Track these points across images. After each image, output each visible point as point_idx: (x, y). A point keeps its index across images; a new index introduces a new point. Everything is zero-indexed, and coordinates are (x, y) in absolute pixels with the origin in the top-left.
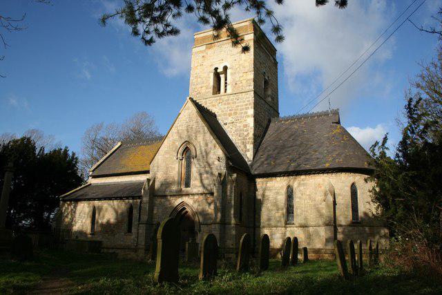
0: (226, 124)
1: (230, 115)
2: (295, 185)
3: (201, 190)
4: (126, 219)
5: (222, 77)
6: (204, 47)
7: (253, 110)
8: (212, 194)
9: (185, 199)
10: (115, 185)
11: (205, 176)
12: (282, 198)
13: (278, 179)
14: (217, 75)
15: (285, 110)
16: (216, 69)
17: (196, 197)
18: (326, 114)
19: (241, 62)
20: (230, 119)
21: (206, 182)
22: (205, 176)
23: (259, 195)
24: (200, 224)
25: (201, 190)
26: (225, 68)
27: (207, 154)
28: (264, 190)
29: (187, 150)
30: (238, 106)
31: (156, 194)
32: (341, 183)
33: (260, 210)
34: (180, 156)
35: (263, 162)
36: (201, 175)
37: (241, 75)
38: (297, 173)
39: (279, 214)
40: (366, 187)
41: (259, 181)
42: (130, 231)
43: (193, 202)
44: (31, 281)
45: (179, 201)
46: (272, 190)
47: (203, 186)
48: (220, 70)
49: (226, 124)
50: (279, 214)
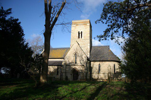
0: (82, 47)
1: (83, 45)
2: (100, 64)
3: (80, 64)
4: (57, 71)
5: (80, 34)
6: (75, 25)
7: (89, 44)
8: (83, 66)
9: (76, 67)
10: (57, 61)
11: (81, 61)
12: (98, 67)
13: (97, 62)
14: (79, 33)
15: (93, 45)
16: (79, 32)
17: (79, 66)
18: (106, 46)
19: (86, 31)
20: (83, 46)
21: (82, 62)
22: (81, 61)
23: (92, 65)
24: (80, 73)
25: (80, 64)
26: (82, 32)
27: (82, 55)
28: (93, 65)
29: (75, 54)
30: (85, 43)
31: (68, 65)
32: (112, 64)
33: (92, 70)
34: (74, 55)
35: (92, 58)
36: (80, 61)
37: (86, 34)
38: (102, 61)
39: (97, 71)
40: (117, 65)
41: (92, 63)
42: (58, 74)
43: (78, 67)
44: (27, 85)
45: (74, 67)
46: (95, 65)
47: (81, 63)
48: (80, 32)
49: (82, 47)
50: (97, 71)
